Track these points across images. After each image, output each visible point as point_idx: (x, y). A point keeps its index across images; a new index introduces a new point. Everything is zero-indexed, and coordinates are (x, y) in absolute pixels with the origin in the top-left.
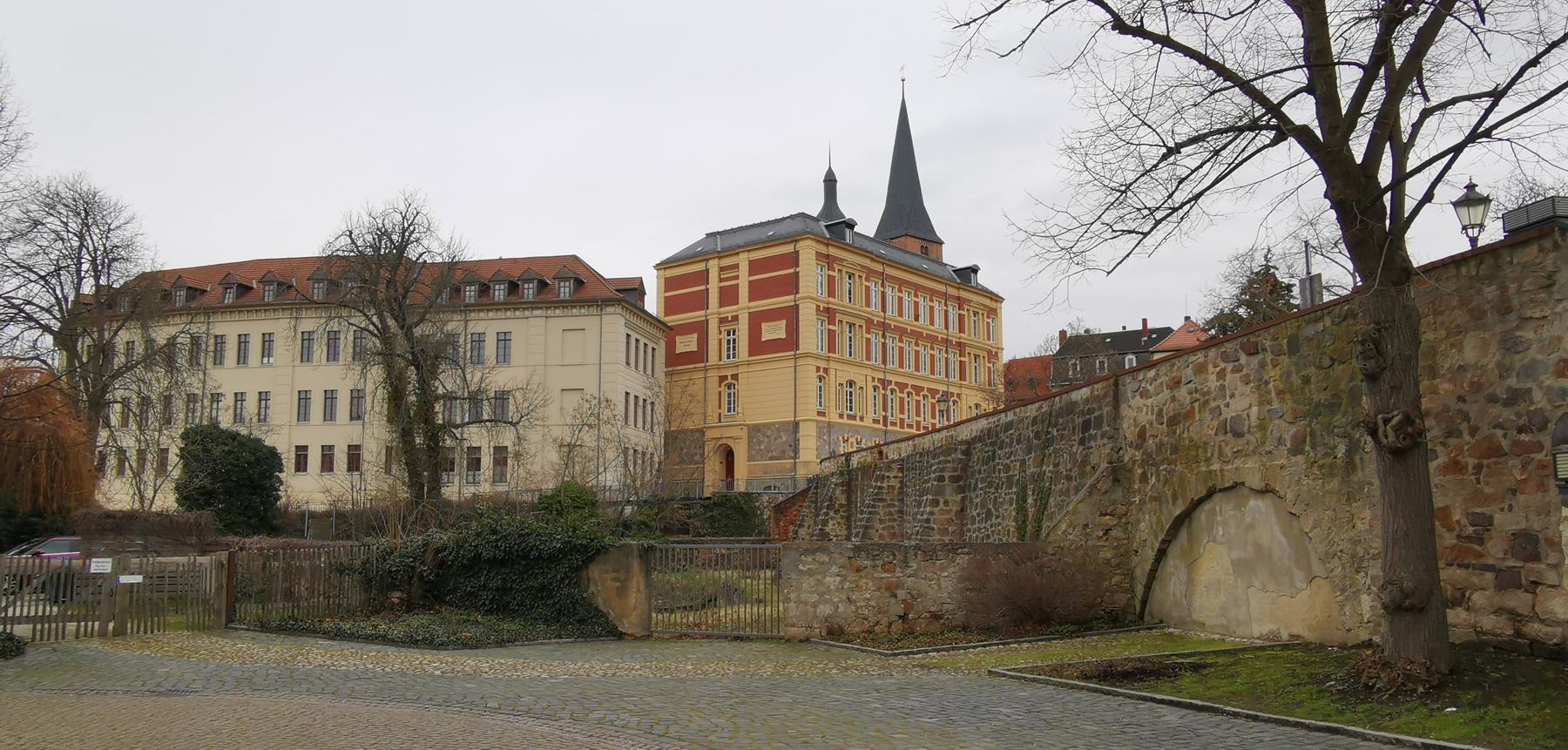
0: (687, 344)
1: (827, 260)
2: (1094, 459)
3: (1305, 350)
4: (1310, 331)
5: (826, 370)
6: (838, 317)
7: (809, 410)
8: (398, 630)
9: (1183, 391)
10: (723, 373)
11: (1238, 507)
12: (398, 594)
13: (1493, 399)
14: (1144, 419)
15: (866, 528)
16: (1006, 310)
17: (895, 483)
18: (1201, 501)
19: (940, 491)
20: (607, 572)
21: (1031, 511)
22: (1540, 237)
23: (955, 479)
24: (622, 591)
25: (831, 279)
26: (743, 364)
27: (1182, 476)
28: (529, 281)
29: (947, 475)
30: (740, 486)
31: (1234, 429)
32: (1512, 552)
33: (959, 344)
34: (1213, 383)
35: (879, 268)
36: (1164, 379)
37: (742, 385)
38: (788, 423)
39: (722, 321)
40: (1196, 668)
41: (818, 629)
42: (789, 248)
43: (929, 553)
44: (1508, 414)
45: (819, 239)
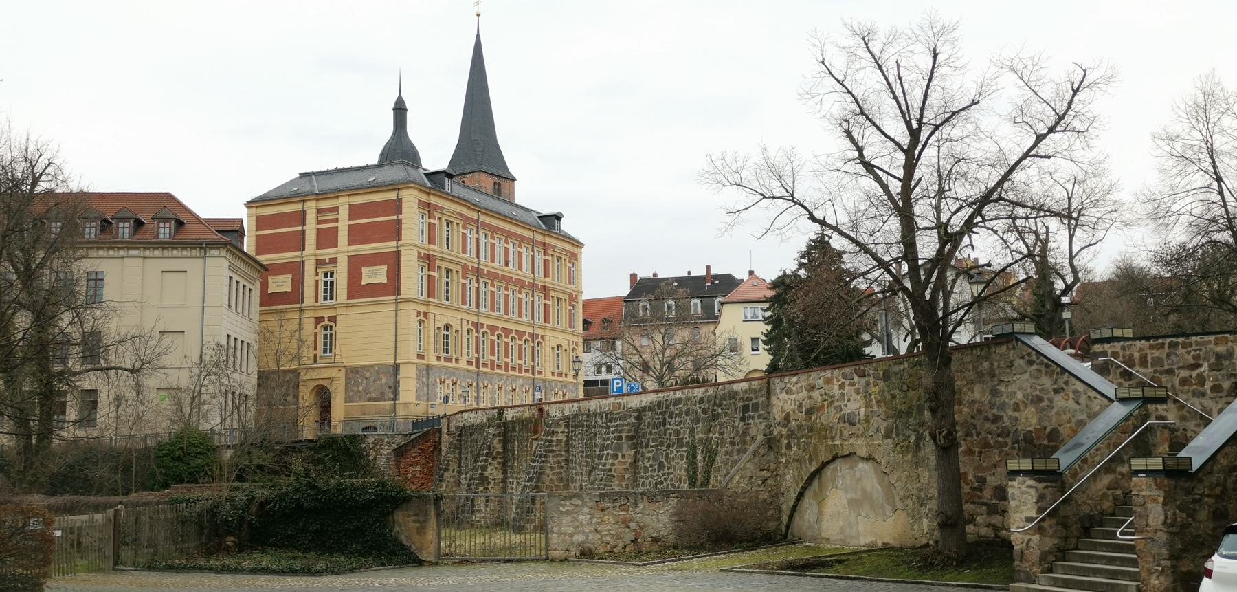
0: (281, 284)
1: (428, 208)
2: (753, 432)
3: (893, 379)
4: (896, 369)
5: (425, 315)
6: (438, 263)
7: (409, 353)
9: (816, 394)
11: (851, 468)
12: (232, 539)
13: (987, 419)
14: (789, 408)
15: (540, 474)
16: (585, 254)
17: (562, 437)
18: (828, 463)
19: (619, 448)
21: (700, 465)
22: (1007, 342)
23: (630, 438)
24: (422, 530)
26: (341, 306)
27: (815, 448)
28: (124, 220)
29: (624, 435)
31: (850, 420)
32: (995, 496)
34: (836, 391)
35: (474, 215)
36: (803, 384)
38: (388, 365)
39: (320, 263)
40: (840, 562)
41: (574, 552)
42: (391, 196)
43: (651, 498)
44: (993, 427)
45: (421, 188)
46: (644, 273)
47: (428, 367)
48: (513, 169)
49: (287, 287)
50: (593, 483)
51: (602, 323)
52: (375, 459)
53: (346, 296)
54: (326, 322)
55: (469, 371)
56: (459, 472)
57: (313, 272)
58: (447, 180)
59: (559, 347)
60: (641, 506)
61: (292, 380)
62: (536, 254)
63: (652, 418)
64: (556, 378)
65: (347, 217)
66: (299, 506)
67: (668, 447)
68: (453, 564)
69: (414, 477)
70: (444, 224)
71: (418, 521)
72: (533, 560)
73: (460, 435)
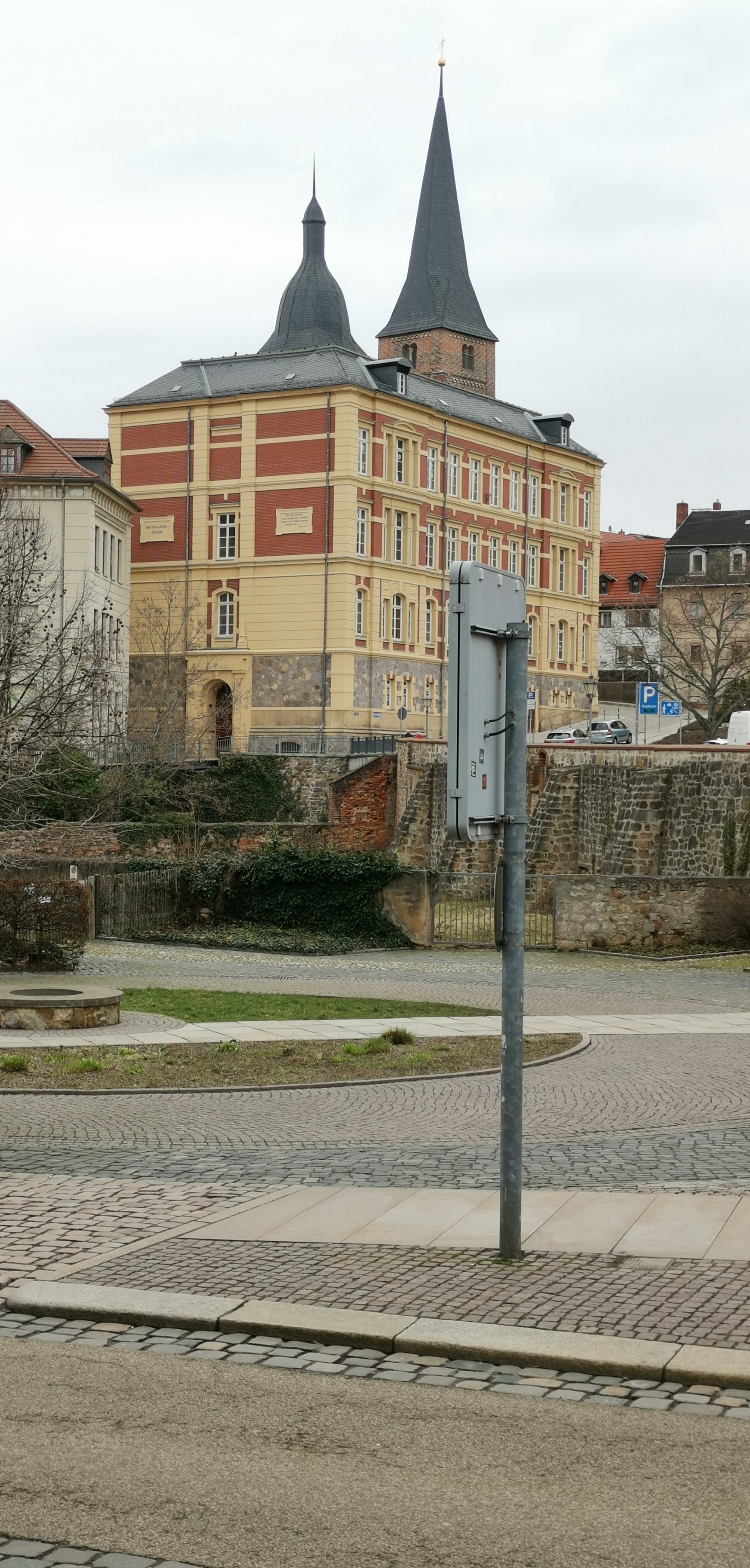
0: (159, 529)
1: (373, 421)
5: (368, 581)
6: (386, 503)
7: (343, 640)
8: (271, 942)
10: (215, 576)
15: (542, 839)
16: (606, 478)
19: (642, 816)
20: (400, 894)
24: (414, 910)
25: (377, 449)
29: (649, 801)
30: (241, 742)
33: (542, 534)
35: (438, 427)
37: (245, 597)
38: (314, 655)
39: (214, 500)
41: (585, 942)
42: (319, 403)
43: (675, 886)
45: (364, 392)
46: (699, 503)
47: (371, 659)
48: (493, 322)
49: (168, 535)
50: (609, 857)
51: (635, 577)
52: (299, 791)
53: (252, 552)
54: (224, 588)
55: (428, 663)
56: (429, 824)
57: (205, 514)
58: (399, 375)
59: (562, 623)
60: (664, 894)
61: (176, 669)
62: (530, 482)
63: (684, 782)
64: (556, 671)
65: (254, 433)
66: (278, 878)
67: (703, 820)
68: (448, 948)
69: (360, 822)
70: (395, 443)
71: (410, 901)
72: (538, 949)
73: (431, 776)
